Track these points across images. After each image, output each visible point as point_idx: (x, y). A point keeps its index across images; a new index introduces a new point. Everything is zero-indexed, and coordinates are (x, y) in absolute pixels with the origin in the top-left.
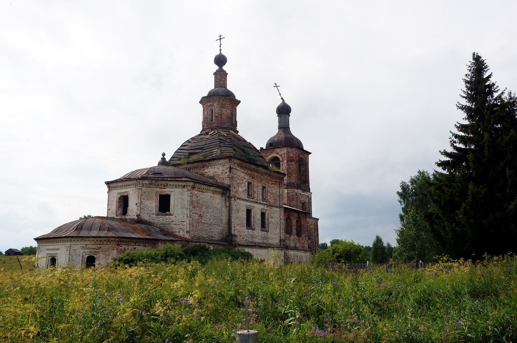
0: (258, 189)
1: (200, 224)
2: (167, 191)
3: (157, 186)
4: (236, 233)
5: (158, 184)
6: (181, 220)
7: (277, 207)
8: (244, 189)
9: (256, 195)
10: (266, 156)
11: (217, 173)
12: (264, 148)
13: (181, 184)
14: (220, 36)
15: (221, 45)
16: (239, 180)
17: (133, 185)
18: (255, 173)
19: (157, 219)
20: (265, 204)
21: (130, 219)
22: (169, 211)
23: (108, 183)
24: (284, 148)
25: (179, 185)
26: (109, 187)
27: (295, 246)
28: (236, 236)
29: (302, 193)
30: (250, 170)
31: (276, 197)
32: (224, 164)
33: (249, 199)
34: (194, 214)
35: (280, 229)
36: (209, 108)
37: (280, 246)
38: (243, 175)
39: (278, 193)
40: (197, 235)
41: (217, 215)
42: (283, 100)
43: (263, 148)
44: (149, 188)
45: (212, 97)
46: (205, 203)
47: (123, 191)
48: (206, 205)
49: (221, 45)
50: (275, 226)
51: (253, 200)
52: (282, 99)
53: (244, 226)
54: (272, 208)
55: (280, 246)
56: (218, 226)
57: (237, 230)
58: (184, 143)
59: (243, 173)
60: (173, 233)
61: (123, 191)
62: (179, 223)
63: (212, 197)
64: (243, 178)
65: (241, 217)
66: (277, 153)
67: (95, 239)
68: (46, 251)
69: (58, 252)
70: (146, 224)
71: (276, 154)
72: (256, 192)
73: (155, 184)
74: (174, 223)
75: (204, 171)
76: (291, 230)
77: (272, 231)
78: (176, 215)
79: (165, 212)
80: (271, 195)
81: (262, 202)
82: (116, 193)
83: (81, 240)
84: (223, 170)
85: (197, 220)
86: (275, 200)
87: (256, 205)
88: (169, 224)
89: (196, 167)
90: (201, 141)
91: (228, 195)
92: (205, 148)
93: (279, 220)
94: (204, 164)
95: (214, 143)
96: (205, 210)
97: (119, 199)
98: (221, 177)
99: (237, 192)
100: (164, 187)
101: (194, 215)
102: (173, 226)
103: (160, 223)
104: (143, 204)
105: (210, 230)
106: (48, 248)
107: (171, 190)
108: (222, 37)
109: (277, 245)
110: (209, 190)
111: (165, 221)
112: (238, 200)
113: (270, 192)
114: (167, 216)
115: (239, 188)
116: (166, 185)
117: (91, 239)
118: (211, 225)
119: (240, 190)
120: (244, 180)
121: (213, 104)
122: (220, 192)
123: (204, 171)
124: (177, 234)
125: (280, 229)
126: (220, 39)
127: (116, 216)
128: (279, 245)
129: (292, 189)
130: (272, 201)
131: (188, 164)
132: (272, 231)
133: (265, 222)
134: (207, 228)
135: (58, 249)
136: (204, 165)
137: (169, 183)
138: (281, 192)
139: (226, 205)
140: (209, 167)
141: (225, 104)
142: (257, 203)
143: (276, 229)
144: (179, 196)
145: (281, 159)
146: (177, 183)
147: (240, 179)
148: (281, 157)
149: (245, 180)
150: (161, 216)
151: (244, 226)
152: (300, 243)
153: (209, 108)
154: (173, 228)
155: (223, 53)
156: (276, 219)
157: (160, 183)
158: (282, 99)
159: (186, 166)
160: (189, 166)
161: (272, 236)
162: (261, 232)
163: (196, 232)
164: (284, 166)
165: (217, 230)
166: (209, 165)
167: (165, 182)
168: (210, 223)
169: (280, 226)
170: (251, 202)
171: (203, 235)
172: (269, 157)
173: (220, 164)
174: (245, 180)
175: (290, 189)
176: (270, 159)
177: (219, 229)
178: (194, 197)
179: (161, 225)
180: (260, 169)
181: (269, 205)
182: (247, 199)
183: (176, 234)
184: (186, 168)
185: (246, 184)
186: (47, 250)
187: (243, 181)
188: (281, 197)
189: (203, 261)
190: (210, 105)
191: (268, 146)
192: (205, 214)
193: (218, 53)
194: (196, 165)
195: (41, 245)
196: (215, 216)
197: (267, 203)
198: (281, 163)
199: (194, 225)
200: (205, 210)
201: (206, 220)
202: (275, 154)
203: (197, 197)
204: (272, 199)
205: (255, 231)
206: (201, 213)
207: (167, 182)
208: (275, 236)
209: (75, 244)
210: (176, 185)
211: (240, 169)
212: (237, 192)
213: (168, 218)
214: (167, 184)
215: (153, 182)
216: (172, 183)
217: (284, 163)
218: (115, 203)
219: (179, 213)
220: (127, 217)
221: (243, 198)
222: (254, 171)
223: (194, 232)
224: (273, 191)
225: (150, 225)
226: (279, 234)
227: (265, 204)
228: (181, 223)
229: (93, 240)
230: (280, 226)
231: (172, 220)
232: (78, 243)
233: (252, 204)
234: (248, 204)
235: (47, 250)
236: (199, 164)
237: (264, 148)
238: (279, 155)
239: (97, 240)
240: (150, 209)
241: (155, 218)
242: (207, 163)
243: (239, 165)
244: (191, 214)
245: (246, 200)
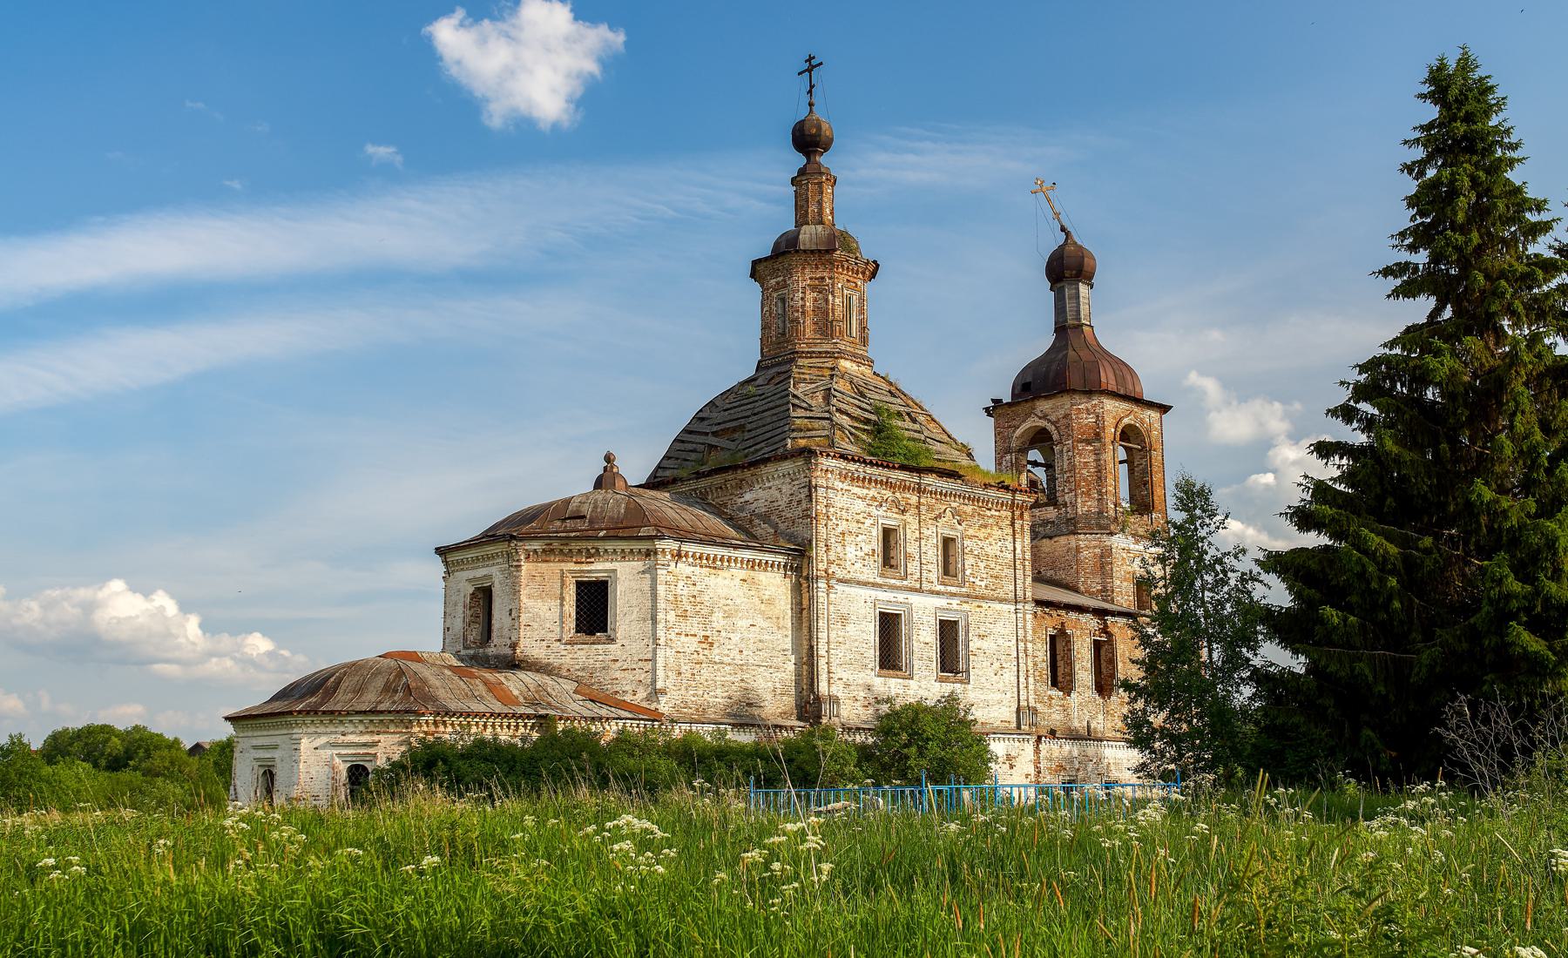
0: (920, 542)
1: (703, 665)
2: (598, 568)
3: (566, 555)
4: (835, 693)
5: (570, 550)
6: (641, 657)
7: (1006, 600)
8: (867, 549)
9: (913, 567)
10: (1010, 427)
11: (775, 504)
12: (1007, 399)
13: (636, 546)
14: (811, 58)
15: (812, 87)
16: (844, 522)
17: (503, 555)
18: (908, 496)
19: (571, 656)
20: (953, 595)
21: (496, 657)
22: (606, 631)
23: (442, 551)
24: (1062, 399)
25: (632, 550)
26: (446, 563)
27: (1089, 727)
28: (834, 700)
29: (1132, 546)
30: (888, 484)
31: (1000, 567)
32: (794, 474)
33: (888, 580)
34: (683, 636)
35: (1018, 671)
36: (775, 295)
37: (1019, 727)
38: (860, 506)
39: (1010, 556)
40: (693, 699)
41: (767, 637)
42: (1068, 234)
43: (1000, 401)
44: (544, 565)
45: (780, 259)
46: (723, 602)
47: (480, 572)
48: (726, 608)
49: (812, 87)
50: (996, 665)
51: (905, 583)
52: (1063, 229)
53: (870, 666)
54: (984, 605)
55: (1019, 727)
56: (771, 670)
57: (838, 682)
58: (701, 411)
59: (863, 498)
60: (618, 697)
61: (480, 572)
62: (634, 666)
63: (748, 581)
64: (861, 516)
65: (856, 640)
66: (1045, 417)
67: (366, 719)
68: (252, 751)
69: (277, 754)
70: (537, 671)
71: (1040, 418)
72: (917, 557)
73: (561, 550)
74: (618, 664)
75: (742, 500)
76: (1071, 675)
77: (983, 680)
78: (624, 642)
79: (592, 633)
80: (980, 564)
81: (942, 588)
82: (465, 582)
83: (331, 721)
84: (791, 495)
85: (695, 656)
86: (996, 577)
87: (914, 599)
88: (604, 668)
89: (721, 488)
90: (742, 405)
91: (804, 574)
92: (749, 427)
93: (1014, 641)
94: (740, 474)
95: (776, 407)
96: (723, 622)
97: (471, 599)
98: (788, 516)
99: (839, 562)
100: (587, 558)
101: (683, 638)
102: (618, 674)
103: (577, 667)
104: (529, 612)
105: (742, 684)
106: (255, 742)
107: (608, 566)
108: (814, 62)
109: (1007, 725)
110: (736, 560)
111: (591, 661)
112: (840, 587)
113: (976, 553)
114: (599, 647)
115: (848, 549)
116: (593, 551)
117: (356, 718)
118: (745, 668)
119: (849, 556)
120: (866, 521)
121: (785, 281)
122: (779, 565)
123: (742, 500)
124: (628, 698)
125: (1018, 671)
126: (810, 70)
127: (465, 648)
128: (1014, 725)
129: (1091, 534)
130: (983, 584)
131: (697, 478)
132: (983, 680)
133: (957, 652)
134: (729, 678)
135: (275, 747)
136: (742, 480)
137: (601, 545)
138: (1018, 551)
139: (802, 604)
140: (757, 487)
141: (823, 278)
142: (919, 591)
143: (1000, 672)
144: (633, 584)
145: (1055, 437)
146: (626, 546)
147: (849, 518)
148: (1057, 428)
149: (872, 522)
150: (579, 646)
151: (870, 666)
152: (1109, 717)
153: (775, 295)
154: (615, 682)
155: (819, 114)
156: (1000, 641)
157: (575, 546)
158: (1063, 229)
159: (693, 484)
160: (703, 483)
161: (982, 697)
162: (938, 684)
163: (692, 692)
164: (1065, 458)
165: (770, 684)
166: (754, 478)
167: (589, 545)
168: (741, 662)
169: (1018, 663)
170: (893, 588)
171: (717, 700)
172: (1019, 432)
173: (784, 476)
174: (868, 522)
175: (1085, 534)
176: (1022, 435)
177: (777, 680)
178: (681, 584)
179: (579, 673)
180: (930, 480)
181: (968, 596)
182: (879, 580)
183: (625, 698)
184: (695, 490)
185: (874, 533)
186: (255, 747)
187: (860, 525)
188: (1018, 567)
189: (1139, 778)
190: (778, 283)
191: (1016, 392)
192: (723, 634)
193: (803, 113)
194: (718, 479)
195: (242, 735)
196: (760, 641)
197: (964, 590)
198: (1057, 449)
199: (683, 670)
200: (723, 622)
201: (726, 652)
202: (1036, 418)
203: (694, 585)
204: (985, 576)
205: (911, 681)
206: (708, 633)
207: (597, 544)
208: (999, 696)
209: (316, 733)
210: (623, 550)
211: (848, 488)
212: (839, 562)
213: (601, 652)
214: (597, 550)
215: (556, 544)
216: (610, 546)
217: (1065, 449)
218: (460, 609)
219: (633, 634)
220: (491, 651)
221: (862, 578)
222: (906, 488)
223: (683, 692)
224: (988, 549)
225: (549, 673)
226: (1016, 689)
227: (953, 595)
228: (641, 664)
229: (361, 721)
230: (1018, 663)
231: (612, 657)
232: (321, 729)
233: (901, 597)
234: (884, 595)
235: (255, 747)
236: (729, 476)
237: (1007, 399)
238: (1049, 421)
239: (372, 721)
240: (548, 626)
241: (564, 653)
242: (747, 473)
243: (843, 477)
244: (673, 636)
245: (874, 585)
